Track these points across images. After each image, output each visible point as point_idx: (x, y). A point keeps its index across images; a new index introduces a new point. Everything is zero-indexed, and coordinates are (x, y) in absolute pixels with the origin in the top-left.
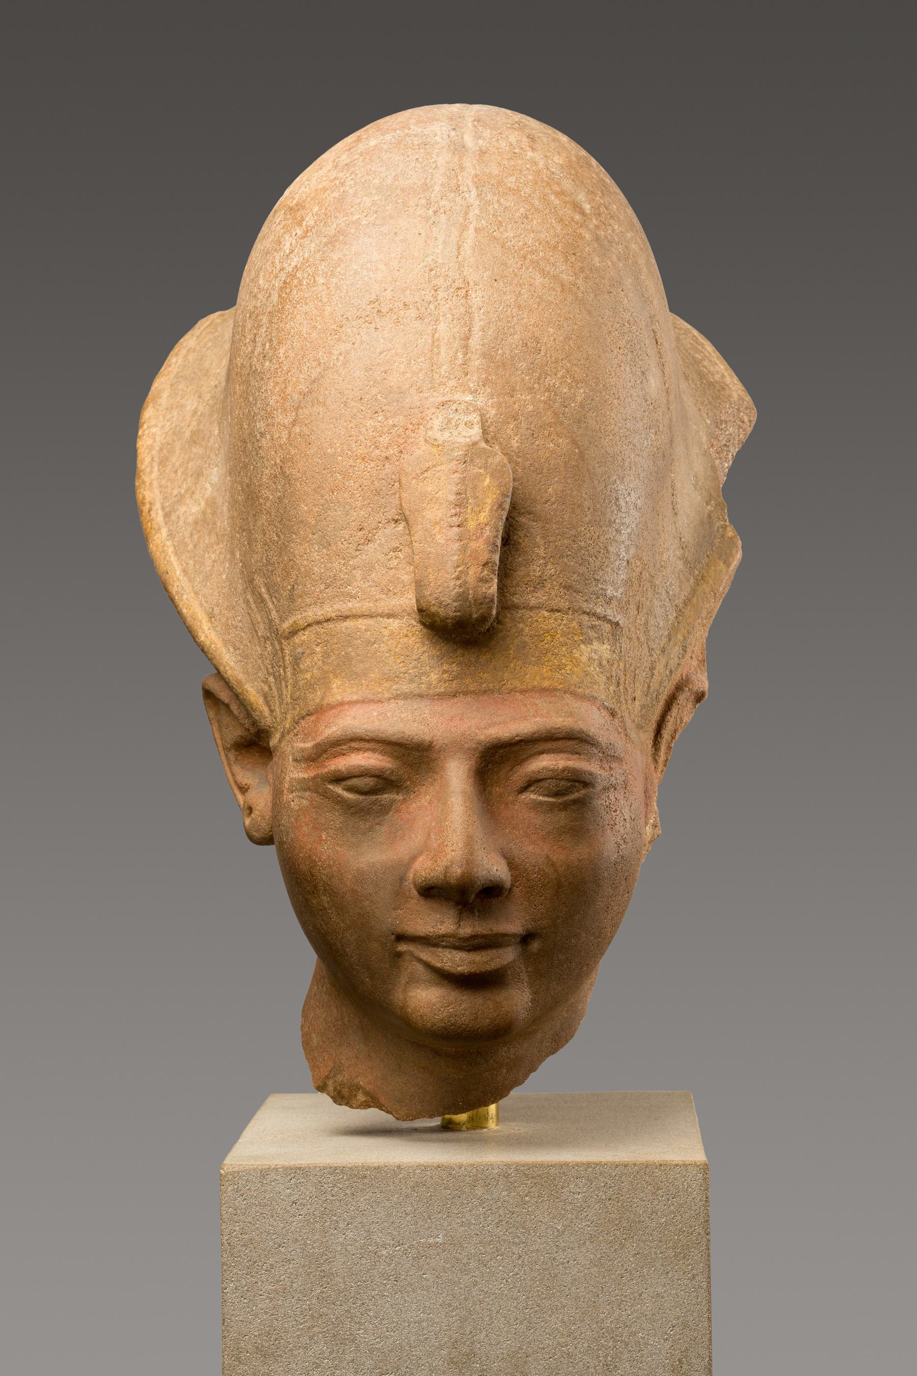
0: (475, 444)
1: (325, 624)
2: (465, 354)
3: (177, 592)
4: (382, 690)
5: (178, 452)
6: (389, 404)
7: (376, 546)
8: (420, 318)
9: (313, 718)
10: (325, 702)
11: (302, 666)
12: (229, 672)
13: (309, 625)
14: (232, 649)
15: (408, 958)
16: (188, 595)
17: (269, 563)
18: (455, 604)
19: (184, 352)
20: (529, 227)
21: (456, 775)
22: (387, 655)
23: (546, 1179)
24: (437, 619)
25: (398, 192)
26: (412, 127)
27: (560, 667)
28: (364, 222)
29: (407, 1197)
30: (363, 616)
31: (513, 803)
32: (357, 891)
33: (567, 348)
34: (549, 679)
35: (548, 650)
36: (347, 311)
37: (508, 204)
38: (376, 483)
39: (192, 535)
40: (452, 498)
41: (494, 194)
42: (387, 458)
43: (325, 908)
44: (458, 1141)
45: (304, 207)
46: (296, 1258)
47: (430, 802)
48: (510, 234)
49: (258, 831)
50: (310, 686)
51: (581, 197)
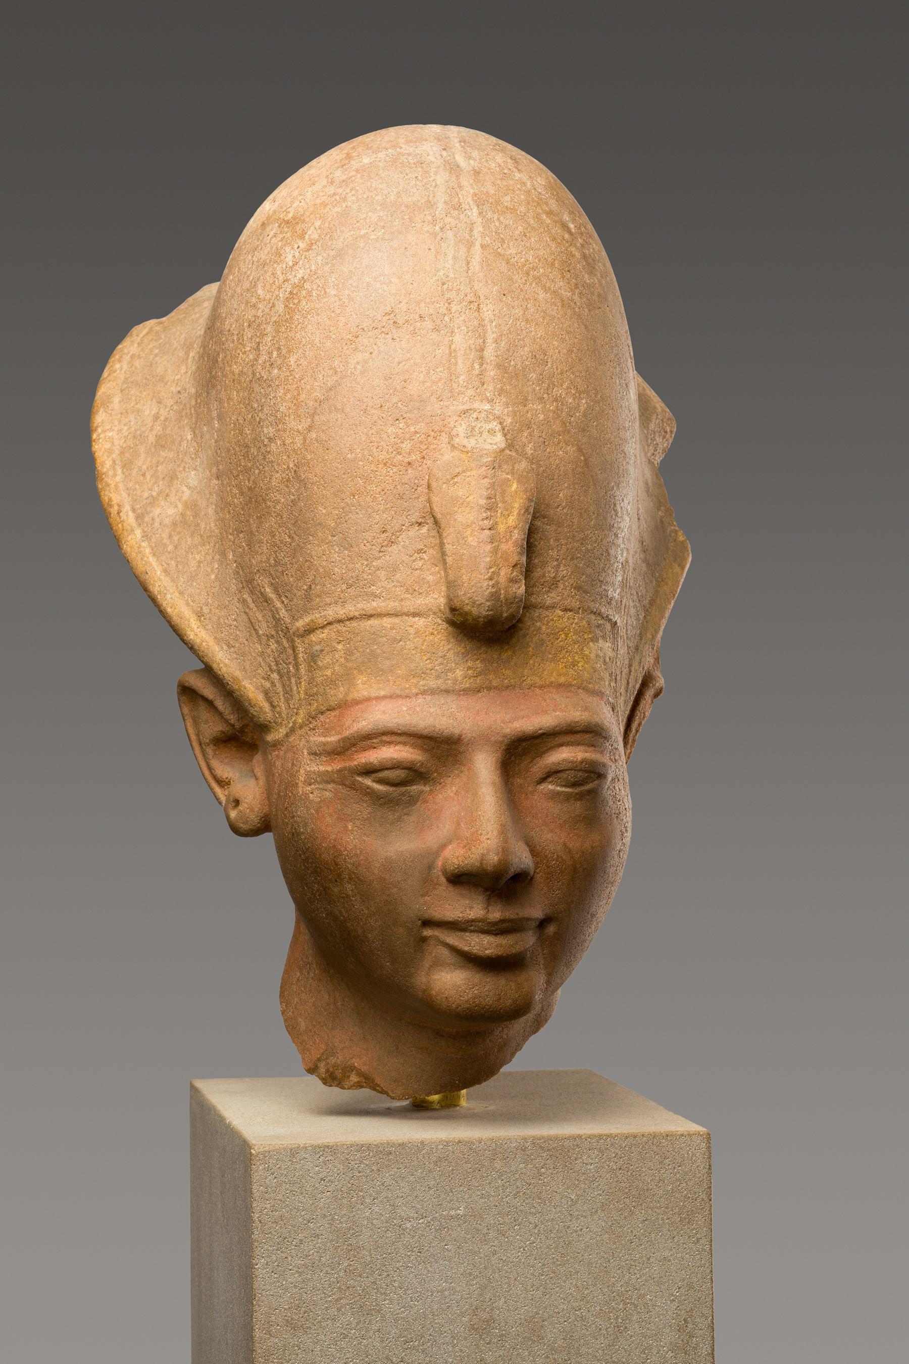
0: (503, 450)
1: (348, 623)
2: (481, 365)
3: (160, 592)
4: (405, 684)
5: (143, 456)
6: (410, 412)
7: (400, 547)
8: (436, 329)
9: (336, 713)
10: (350, 698)
11: (320, 663)
12: (224, 669)
13: (330, 624)
14: (225, 647)
15: (432, 942)
16: (171, 594)
17: (278, 562)
18: (488, 603)
19: (127, 358)
20: (528, 245)
21: (484, 766)
22: (414, 652)
23: (561, 1152)
24: (470, 618)
25: (403, 208)
26: (403, 146)
27: (574, 664)
28: (373, 237)
29: (430, 1171)
30: (388, 615)
31: (532, 793)
32: (385, 879)
33: (570, 360)
34: (565, 675)
35: (563, 648)
36: (362, 322)
37: (507, 222)
38: (399, 487)
39: (170, 536)
40: (483, 502)
41: (494, 212)
42: (409, 463)
43: (348, 896)
44: (429, 1118)
45: (304, 221)
46: (324, 1232)
47: (457, 793)
48: (513, 251)
49: (246, 822)
50: (332, 682)
51: (566, 217)
